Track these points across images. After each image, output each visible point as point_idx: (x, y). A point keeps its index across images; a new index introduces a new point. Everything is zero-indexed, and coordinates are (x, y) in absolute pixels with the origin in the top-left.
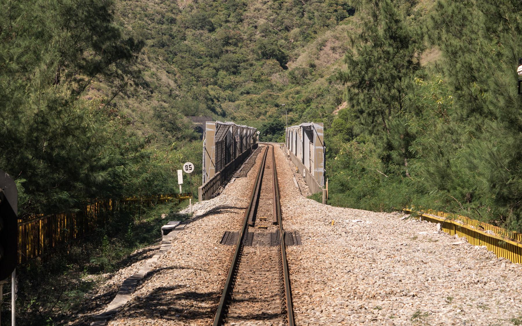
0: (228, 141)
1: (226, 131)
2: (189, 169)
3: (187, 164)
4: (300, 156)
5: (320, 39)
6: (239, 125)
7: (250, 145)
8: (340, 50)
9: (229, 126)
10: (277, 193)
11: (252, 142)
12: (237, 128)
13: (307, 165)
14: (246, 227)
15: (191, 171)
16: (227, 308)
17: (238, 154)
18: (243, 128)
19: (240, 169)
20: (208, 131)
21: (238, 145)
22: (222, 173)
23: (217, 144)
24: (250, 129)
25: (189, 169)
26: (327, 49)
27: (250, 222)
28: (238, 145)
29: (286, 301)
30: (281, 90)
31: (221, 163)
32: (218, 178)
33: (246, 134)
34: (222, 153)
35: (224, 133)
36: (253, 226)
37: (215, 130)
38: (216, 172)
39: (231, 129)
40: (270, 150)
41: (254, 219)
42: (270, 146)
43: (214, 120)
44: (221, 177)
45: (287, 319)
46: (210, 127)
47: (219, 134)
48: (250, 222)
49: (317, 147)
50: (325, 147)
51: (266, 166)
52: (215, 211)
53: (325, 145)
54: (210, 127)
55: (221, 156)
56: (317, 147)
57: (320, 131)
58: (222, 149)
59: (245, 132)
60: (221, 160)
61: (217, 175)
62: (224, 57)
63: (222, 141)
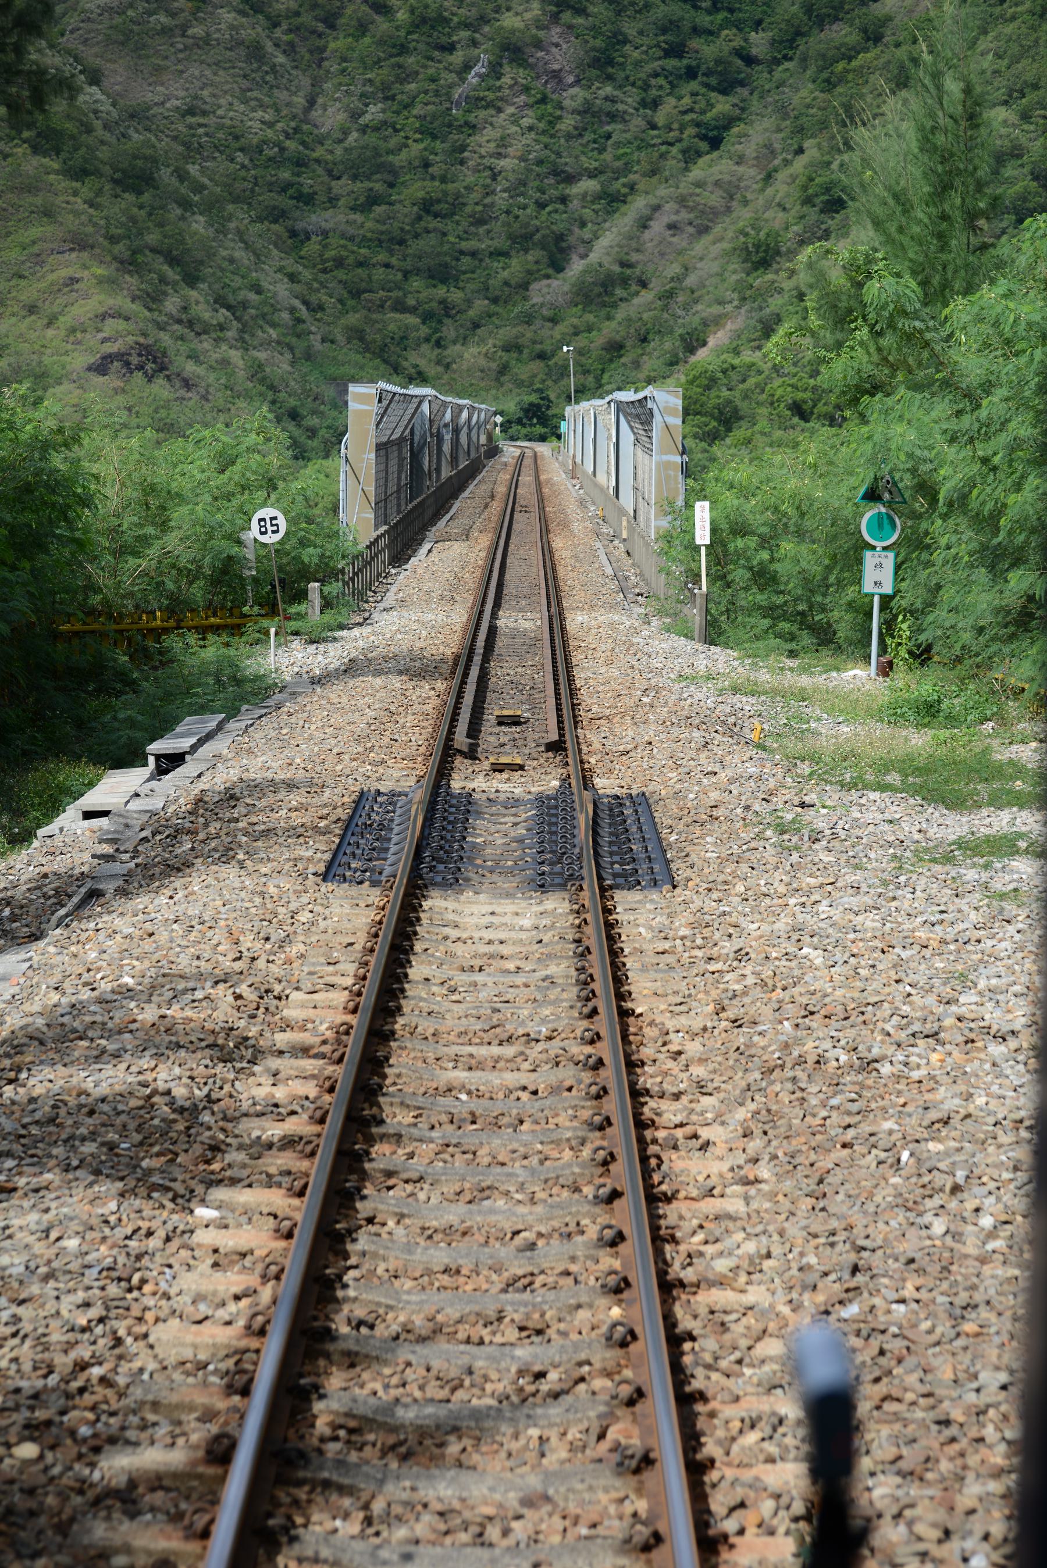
0: (416, 439)
1: (411, 411)
2: (270, 529)
3: (266, 513)
4: (605, 479)
5: (639, 204)
6: (449, 399)
7: (477, 449)
8: (691, 230)
9: (422, 399)
10: (563, 680)
11: (483, 439)
12: (445, 404)
13: (627, 500)
14: (443, 772)
15: (277, 537)
16: (416, 908)
17: (446, 473)
18: (460, 408)
19: (448, 516)
20: (356, 411)
21: (446, 448)
22: (393, 528)
23: (380, 447)
24: (480, 410)
25: (270, 529)
26: (657, 226)
27: (461, 739)
28: (446, 448)
29: (596, 986)
30: (554, 320)
31: (399, 498)
32: (382, 543)
33: (469, 419)
34: (400, 473)
35: (407, 417)
36: (472, 755)
37: (374, 408)
38: (376, 528)
39: (425, 407)
40: (528, 461)
41: (474, 732)
42: (529, 453)
43: (373, 381)
44: (392, 541)
45: (592, 986)
46: (362, 398)
47: (390, 421)
48: (461, 739)
49: (665, 458)
50: (686, 458)
51: (518, 508)
52: (351, 669)
53: (683, 453)
54: (362, 398)
55: (399, 479)
56: (665, 458)
57: (670, 411)
58: (401, 459)
59: (465, 415)
60: (398, 491)
61: (379, 537)
62: (415, 246)
63: (402, 439)
